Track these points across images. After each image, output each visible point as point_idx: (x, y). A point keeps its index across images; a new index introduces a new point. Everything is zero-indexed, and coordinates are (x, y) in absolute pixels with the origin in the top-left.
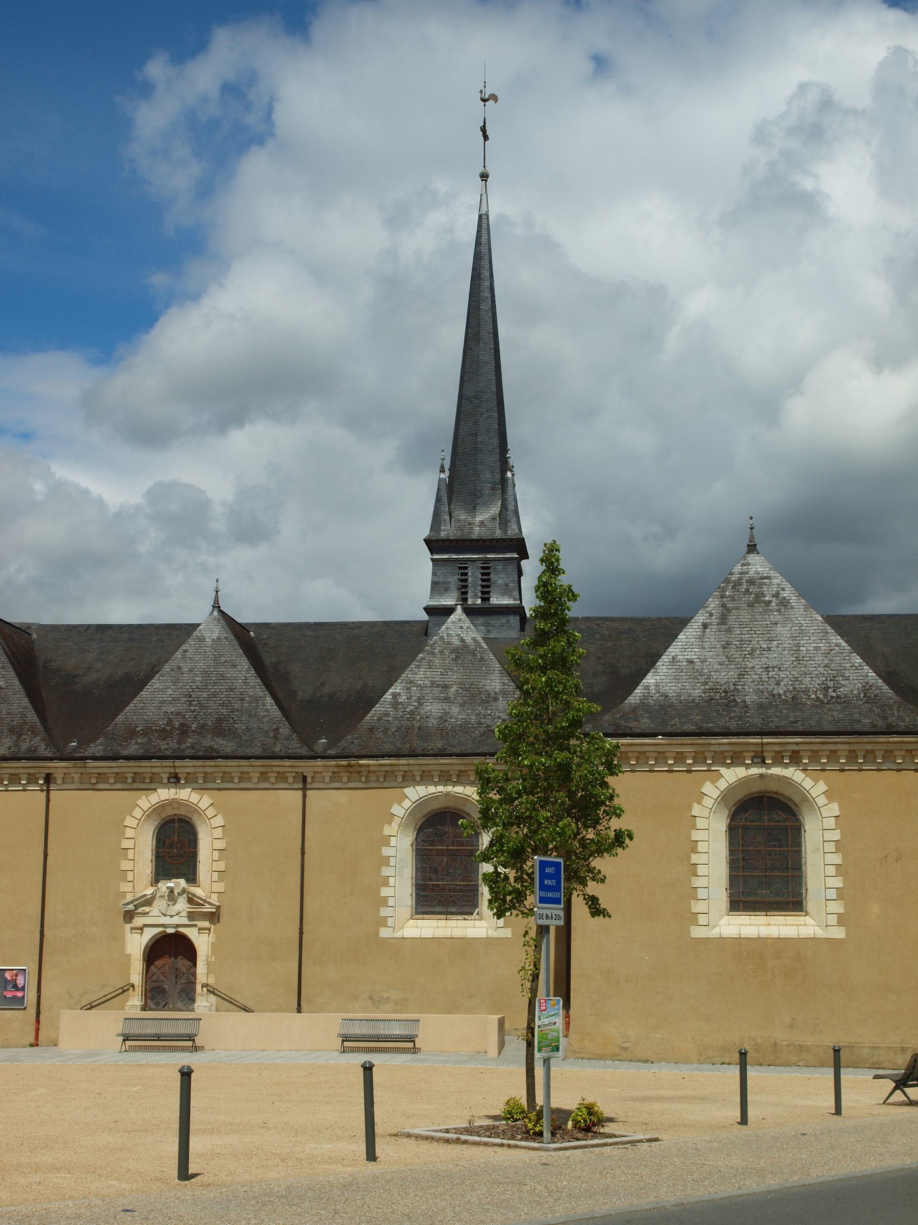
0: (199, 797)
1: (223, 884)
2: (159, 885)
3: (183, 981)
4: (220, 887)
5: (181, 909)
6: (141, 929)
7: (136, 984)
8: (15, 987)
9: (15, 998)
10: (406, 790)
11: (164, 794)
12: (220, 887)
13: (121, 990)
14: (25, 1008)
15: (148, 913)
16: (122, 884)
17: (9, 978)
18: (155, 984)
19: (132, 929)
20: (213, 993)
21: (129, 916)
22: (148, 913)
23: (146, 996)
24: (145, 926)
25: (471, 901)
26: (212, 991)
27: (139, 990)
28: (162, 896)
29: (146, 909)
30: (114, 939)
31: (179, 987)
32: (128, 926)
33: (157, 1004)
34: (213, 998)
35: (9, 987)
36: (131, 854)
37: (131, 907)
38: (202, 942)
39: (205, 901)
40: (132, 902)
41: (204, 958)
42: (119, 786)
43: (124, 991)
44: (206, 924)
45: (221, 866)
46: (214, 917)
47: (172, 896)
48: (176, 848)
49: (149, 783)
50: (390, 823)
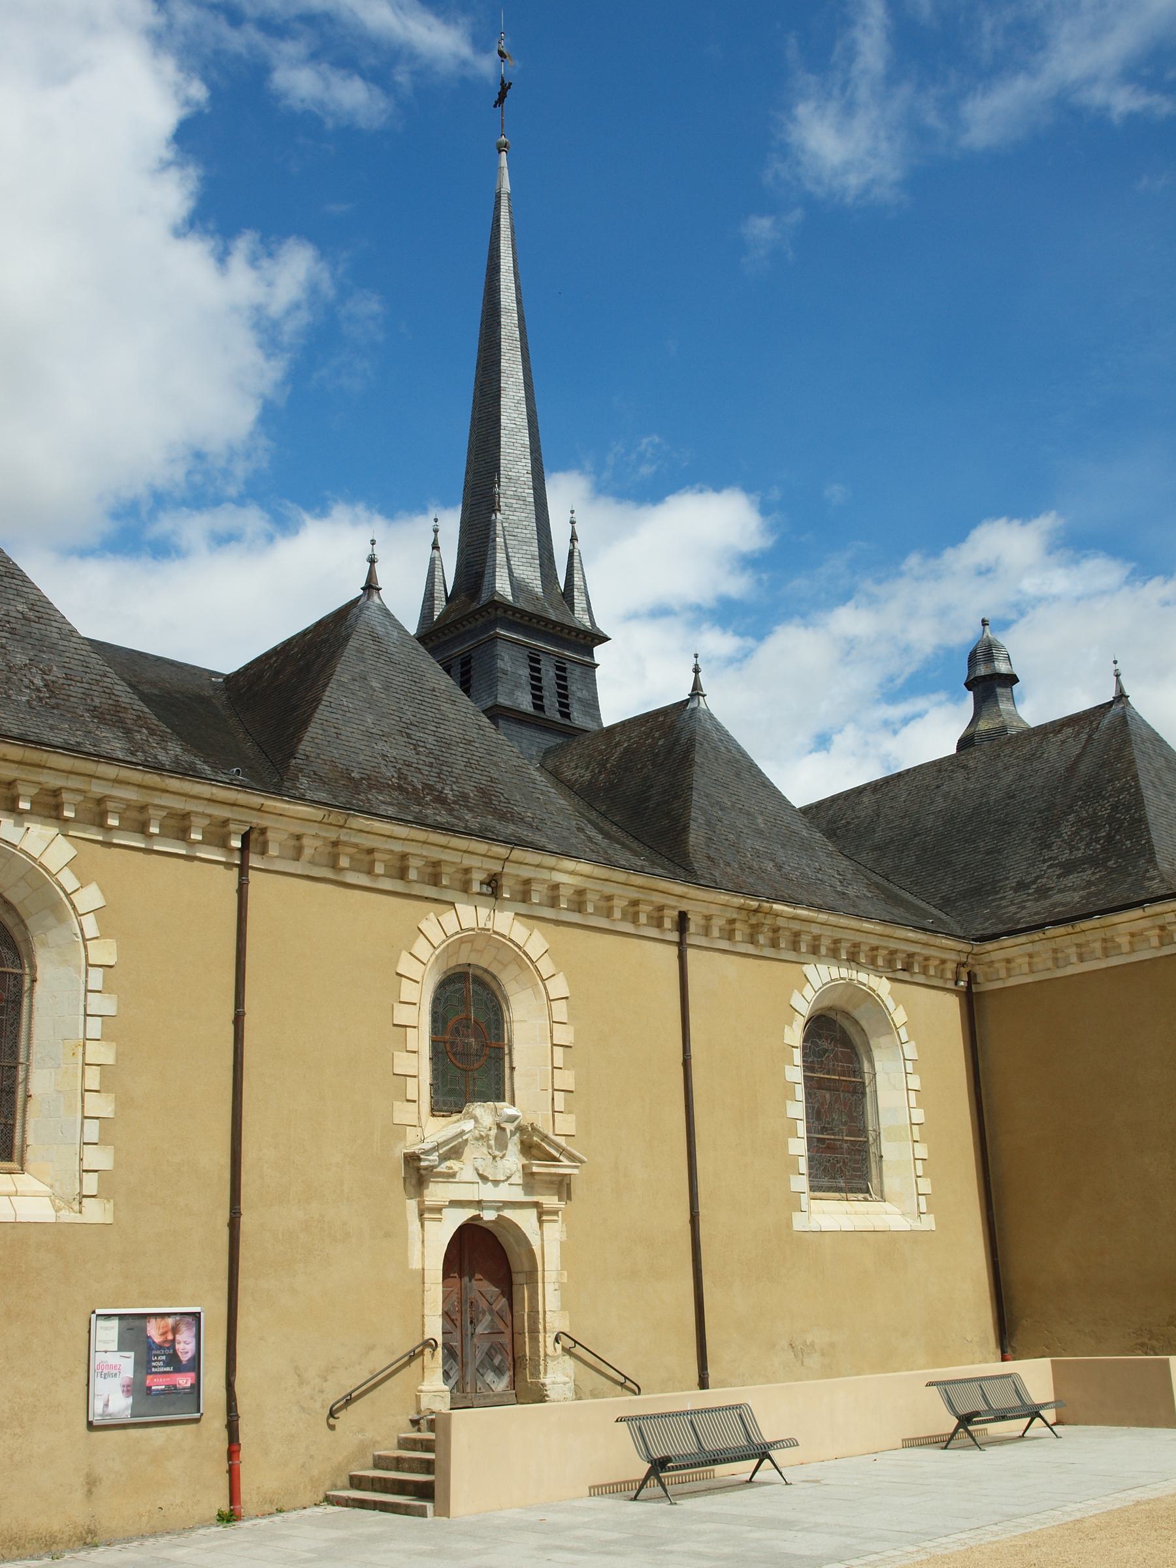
8: (173, 1360)
9: (172, 1390)
10: (809, 969)
11: (470, 915)
13: (622, 1380)
14: (197, 1421)
15: (453, 1175)
17: (158, 1339)
22: (453, 1175)
25: (858, 1170)
26: (571, 1346)
30: (387, 1235)
35: (159, 1365)
38: (547, 1241)
39: (562, 1151)
48: (469, 1042)
49: (436, 883)
50: (791, 1025)
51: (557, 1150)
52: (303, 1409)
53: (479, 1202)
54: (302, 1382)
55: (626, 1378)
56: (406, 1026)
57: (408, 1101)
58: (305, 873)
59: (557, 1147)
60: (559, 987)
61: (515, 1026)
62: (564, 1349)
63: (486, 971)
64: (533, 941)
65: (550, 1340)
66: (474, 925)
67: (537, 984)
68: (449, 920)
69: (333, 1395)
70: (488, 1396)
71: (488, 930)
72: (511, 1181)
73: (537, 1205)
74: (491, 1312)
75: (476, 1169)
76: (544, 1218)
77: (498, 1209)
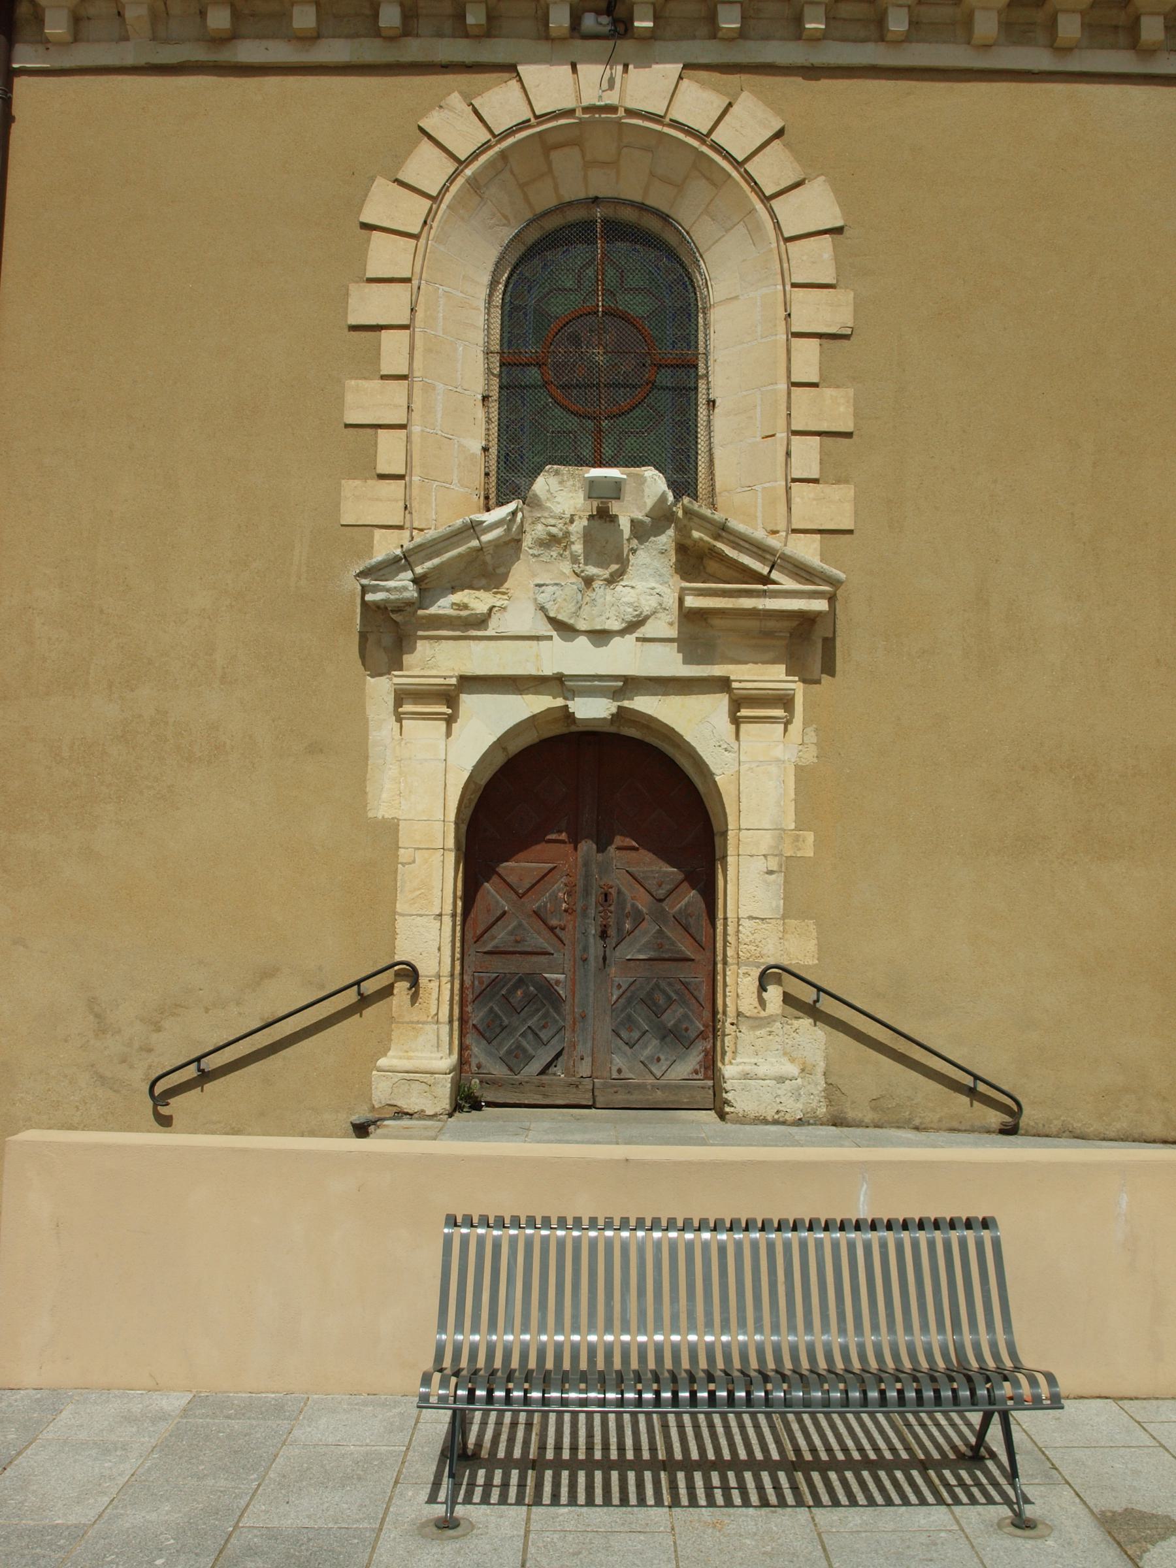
0: (720, 103)
1: (846, 492)
2: (542, 485)
3: (635, 949)
4: (832, 506)
5: (648, 604)
6: (446, 699)
7: (426, 967)
11: (553, 85)
12: (832, 506)
13: (968, 1081)
15: (481, 621)
16: (350, 487)
18: (499, 966)
19: (402, 696)
20: (813, 1012)
21: (388, 632)
22: (481, 621)
23: (463, 1020)
24: (471, 683)
26: (810, 1003)
27: (439, 995)
28: (551, 541)
29: (478, 601)
30: (315, 749)
31: (619, 977)
32: (381, 688)
33: (516, 1058)
34: (811, 1037)
36: (390, 452)
37: (402, 584)
38: (755, 771)
40: (403, 561)
41: (766, 841)
42: (335, 51)
43: (364, 1001)
44: (772, 675)
45: (835, 408)
46: (806, 642)
47: (603, 544)
48: (599, 340)
51: (762, 559)
52: (102, 1079)
53: (559, 679)
54: (103, 1028)
55: (977, 1078)
56: (379, 328)
57: (382, 477)
58: (142, 61)
59: (759, 550)
60: (815, 207)
61: (715, 315)
62: (788, 999)
63: (642, 207)
64: (742, 119)
66: (569, 104)
67: (753, 210)
68: (503, 104)
69: (171, 1049)
70: (640, 1087)
71: (612, 109)
72: (647, 630)
74: (660, 916)
75: (542, 608)
76: (744, 712)
77: (616, 694)
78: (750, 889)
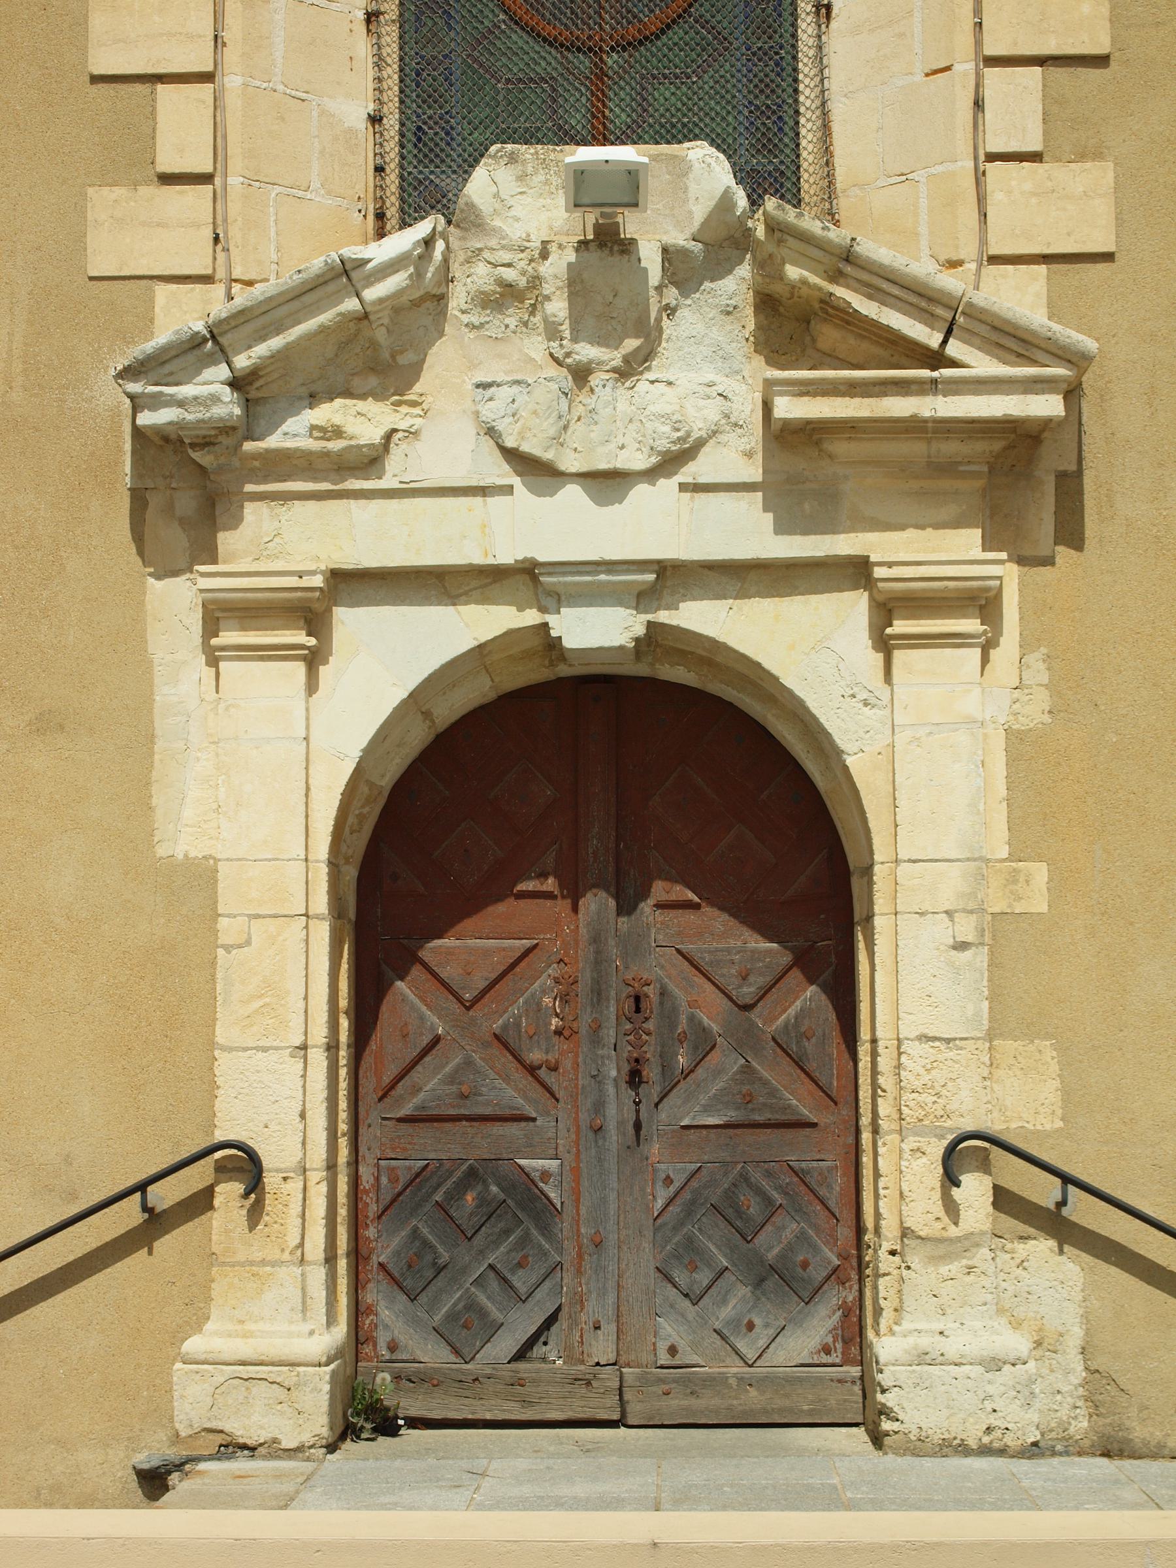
13: (129, 1215)
15: (371, 460)
21: (186, 487)
27: (304, 1205)
29: (361, 420)
32: (176, 600)
38: (923, 745)
39: (956, 317)
44: (951, 551)
46: (1023, 481)
51: (928, 318)
57: (168, 179)
59: (920, 298)
65: (924, 1171)
72: (699, 470)
73: (857, 572)
74: (745, 1040)
75: (491, 432)
76: (900, 626)
77: (643, 598)
78: (920, 976)
